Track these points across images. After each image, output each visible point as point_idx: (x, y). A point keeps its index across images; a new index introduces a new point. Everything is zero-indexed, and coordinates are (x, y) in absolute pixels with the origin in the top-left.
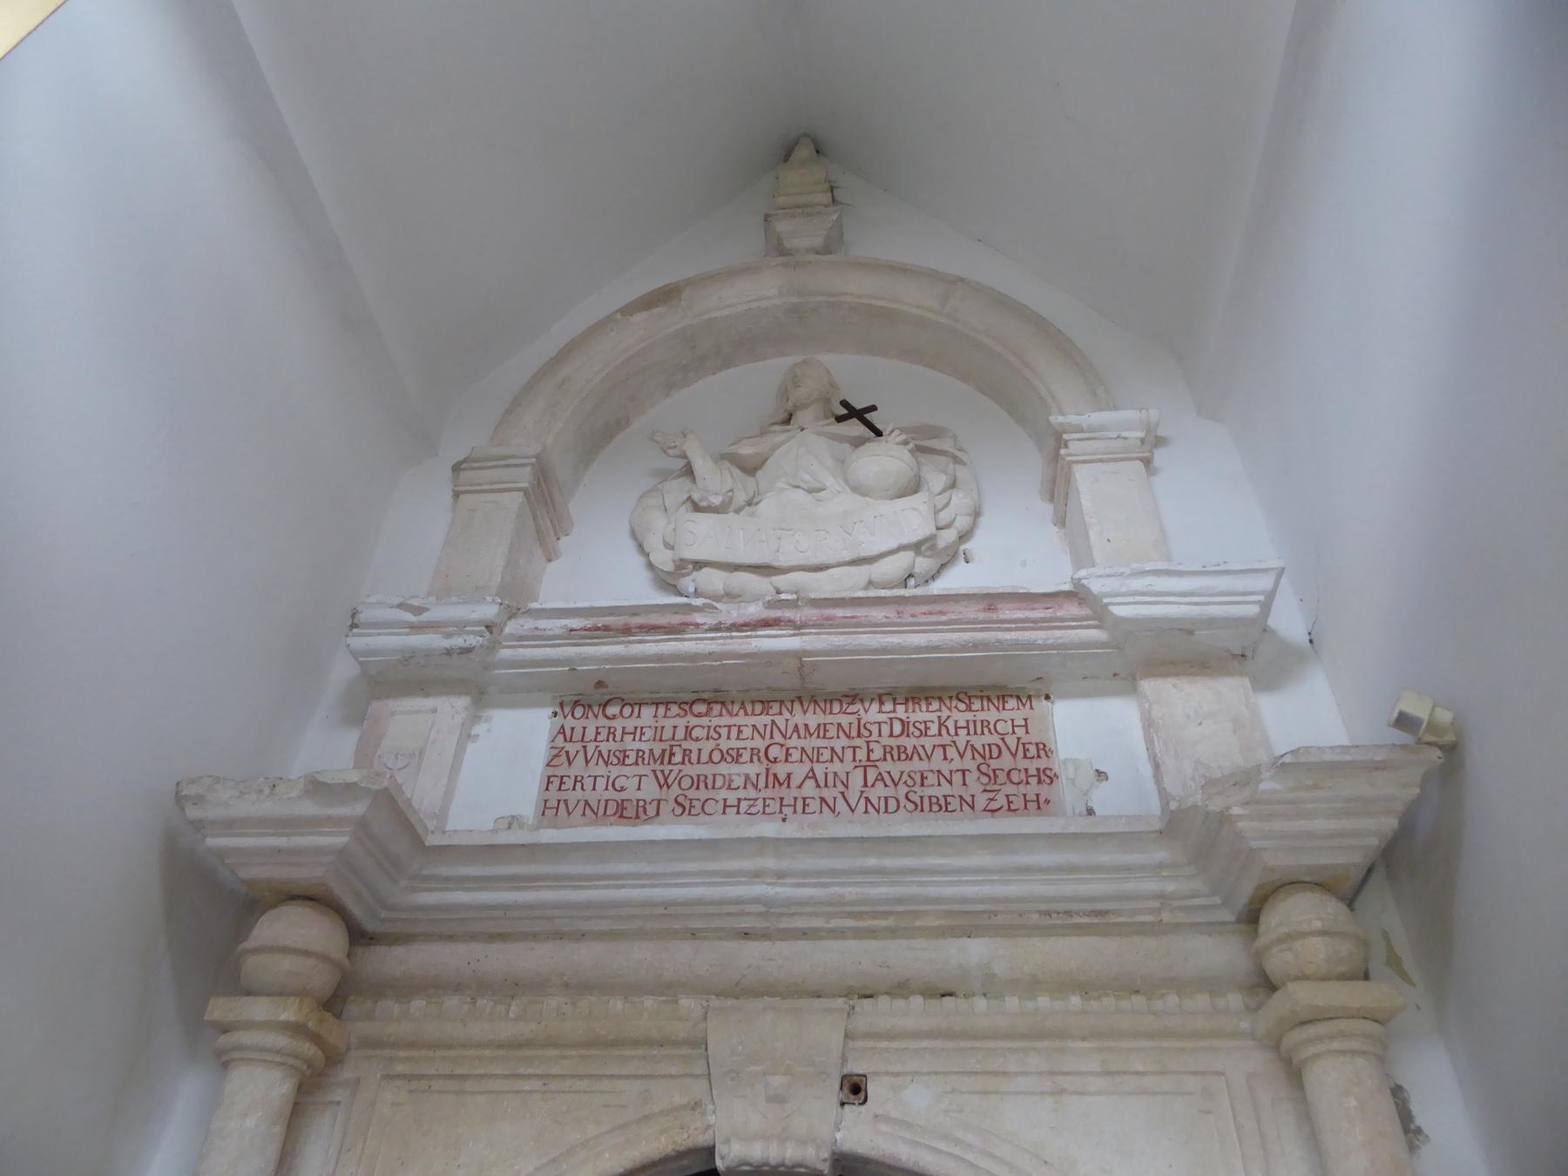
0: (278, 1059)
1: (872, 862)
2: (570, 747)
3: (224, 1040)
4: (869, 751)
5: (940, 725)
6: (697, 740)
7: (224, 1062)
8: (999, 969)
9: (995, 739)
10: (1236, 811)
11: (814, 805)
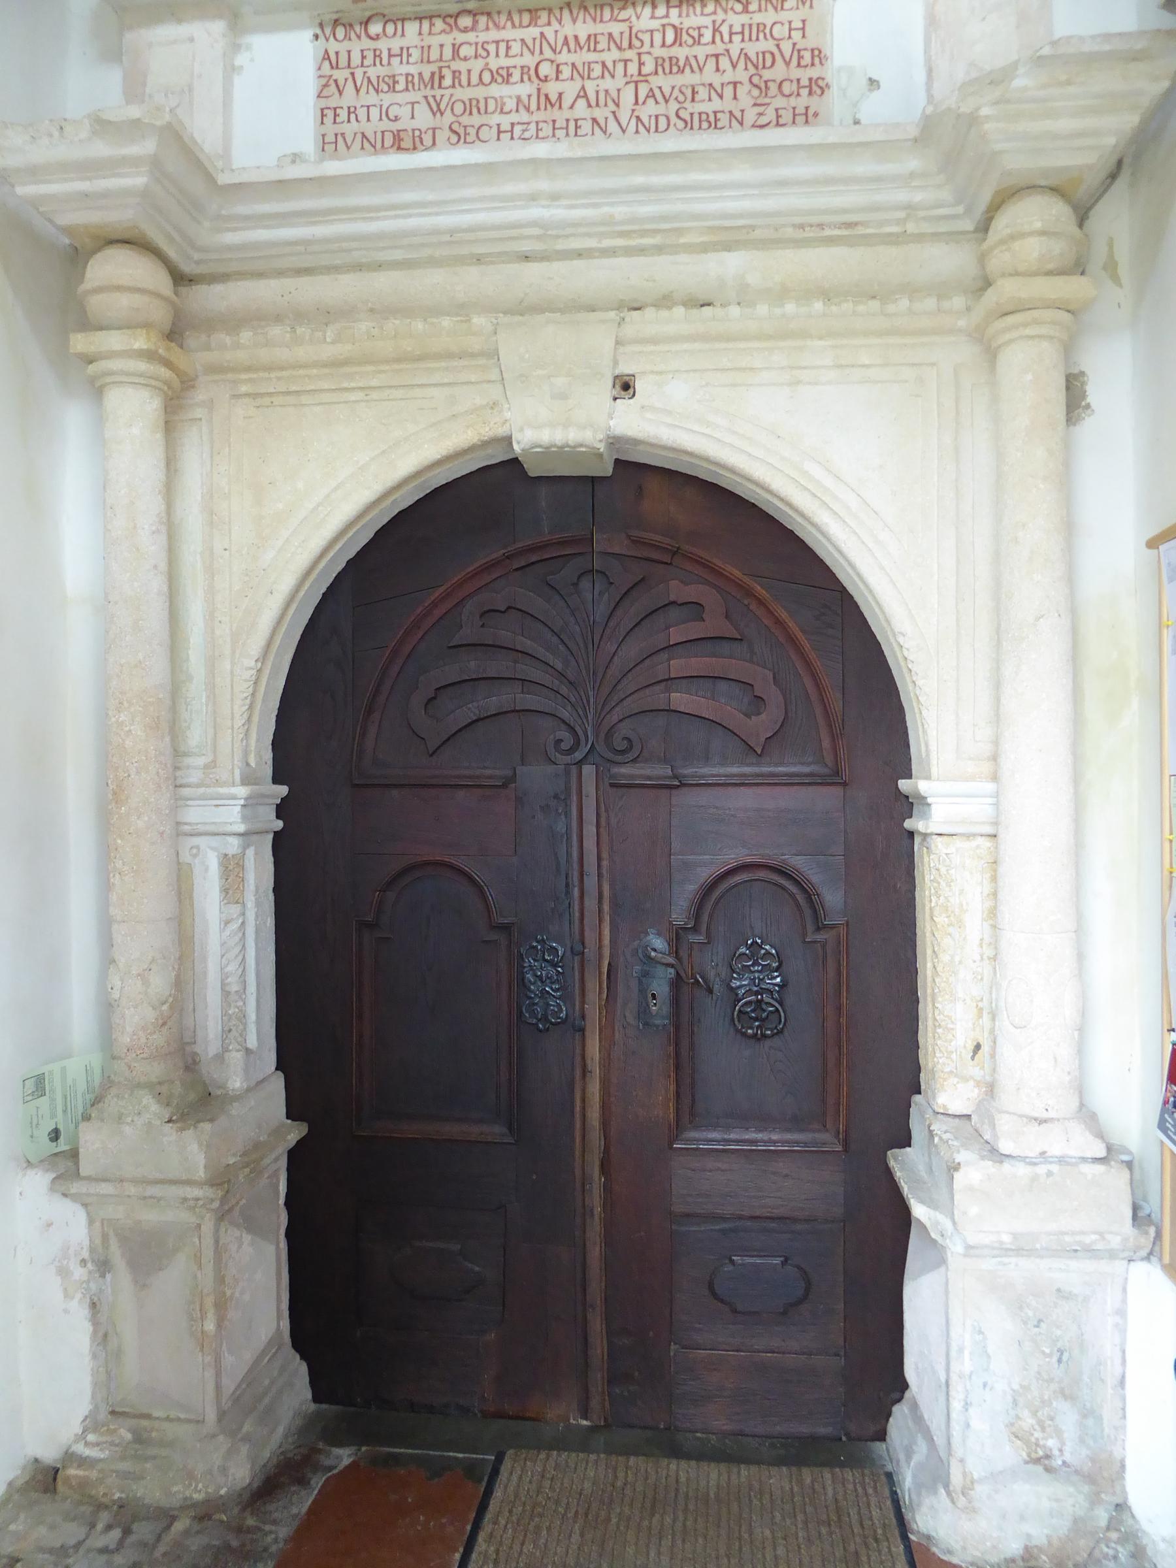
0: (142, 381)
1: (640, 180)
2: (337, 74)
3: (92, 369)
4: (641, 64)
5: (715, 30)
6: (465, 59)
7: (97, 390)
8: (753, 279)
9: (770, 45)
10: (985, 111)
11: (586, 126)
